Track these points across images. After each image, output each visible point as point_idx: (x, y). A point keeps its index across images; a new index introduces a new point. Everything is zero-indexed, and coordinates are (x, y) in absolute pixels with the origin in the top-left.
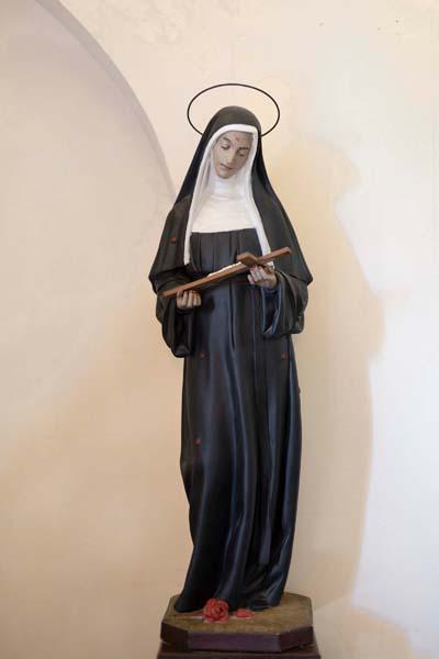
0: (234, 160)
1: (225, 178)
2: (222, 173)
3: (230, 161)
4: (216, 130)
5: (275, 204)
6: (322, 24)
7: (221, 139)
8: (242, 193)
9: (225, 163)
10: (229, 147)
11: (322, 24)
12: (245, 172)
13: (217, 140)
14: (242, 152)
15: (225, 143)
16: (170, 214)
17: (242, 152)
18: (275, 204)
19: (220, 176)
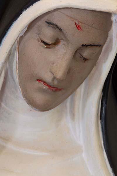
0: (69, 71)
1: (45, 108)
2: (40, 98)
3: (60, 74)
4: (26, 7)
5: (3, 36)
6: (57, 136)
7: (41, 23)
8: (81, 142)
9: (48, 77)
10: (56, 42)
11: (57, 136)
12: (87, 95)
13: (30, 26)
14: (86, 53)
15: (48, 34)
16: (44, 111)
17: (86, 53)
18: (3, 36)
19: (32, 103)
